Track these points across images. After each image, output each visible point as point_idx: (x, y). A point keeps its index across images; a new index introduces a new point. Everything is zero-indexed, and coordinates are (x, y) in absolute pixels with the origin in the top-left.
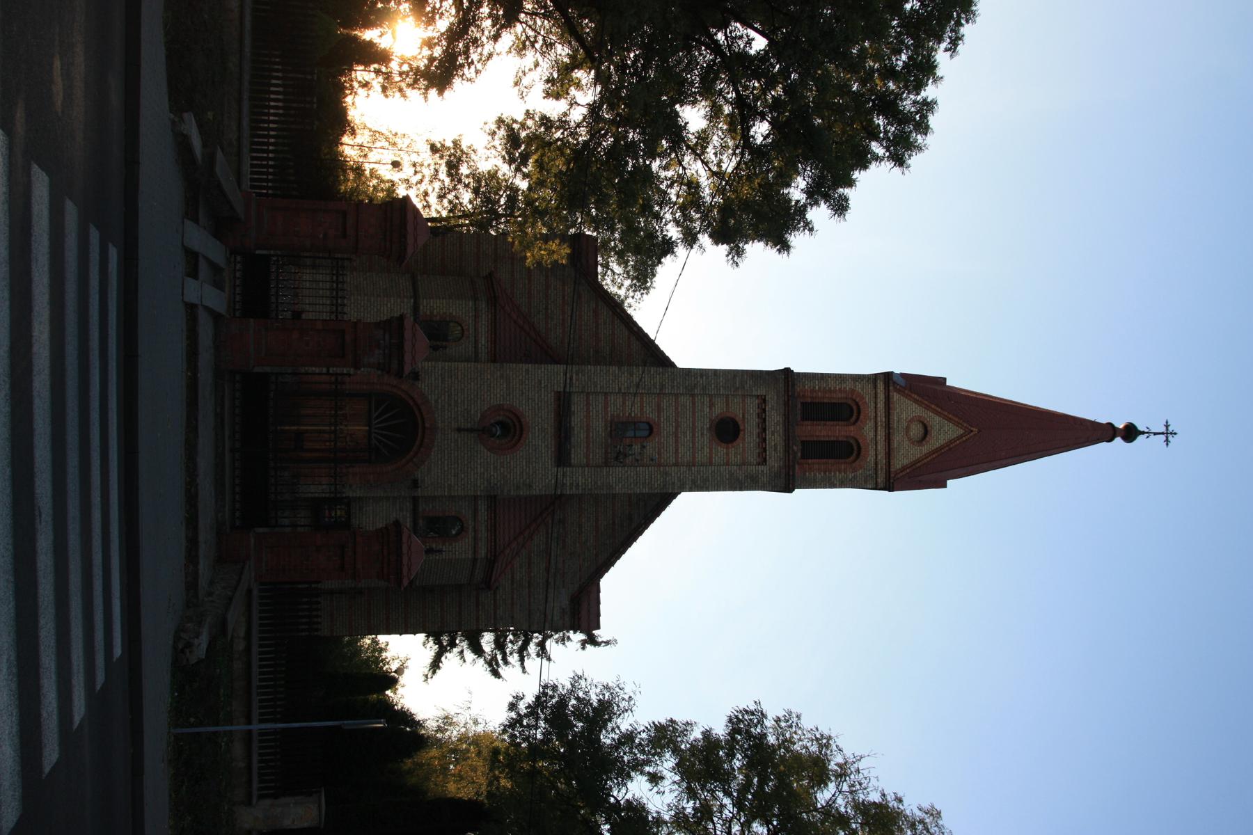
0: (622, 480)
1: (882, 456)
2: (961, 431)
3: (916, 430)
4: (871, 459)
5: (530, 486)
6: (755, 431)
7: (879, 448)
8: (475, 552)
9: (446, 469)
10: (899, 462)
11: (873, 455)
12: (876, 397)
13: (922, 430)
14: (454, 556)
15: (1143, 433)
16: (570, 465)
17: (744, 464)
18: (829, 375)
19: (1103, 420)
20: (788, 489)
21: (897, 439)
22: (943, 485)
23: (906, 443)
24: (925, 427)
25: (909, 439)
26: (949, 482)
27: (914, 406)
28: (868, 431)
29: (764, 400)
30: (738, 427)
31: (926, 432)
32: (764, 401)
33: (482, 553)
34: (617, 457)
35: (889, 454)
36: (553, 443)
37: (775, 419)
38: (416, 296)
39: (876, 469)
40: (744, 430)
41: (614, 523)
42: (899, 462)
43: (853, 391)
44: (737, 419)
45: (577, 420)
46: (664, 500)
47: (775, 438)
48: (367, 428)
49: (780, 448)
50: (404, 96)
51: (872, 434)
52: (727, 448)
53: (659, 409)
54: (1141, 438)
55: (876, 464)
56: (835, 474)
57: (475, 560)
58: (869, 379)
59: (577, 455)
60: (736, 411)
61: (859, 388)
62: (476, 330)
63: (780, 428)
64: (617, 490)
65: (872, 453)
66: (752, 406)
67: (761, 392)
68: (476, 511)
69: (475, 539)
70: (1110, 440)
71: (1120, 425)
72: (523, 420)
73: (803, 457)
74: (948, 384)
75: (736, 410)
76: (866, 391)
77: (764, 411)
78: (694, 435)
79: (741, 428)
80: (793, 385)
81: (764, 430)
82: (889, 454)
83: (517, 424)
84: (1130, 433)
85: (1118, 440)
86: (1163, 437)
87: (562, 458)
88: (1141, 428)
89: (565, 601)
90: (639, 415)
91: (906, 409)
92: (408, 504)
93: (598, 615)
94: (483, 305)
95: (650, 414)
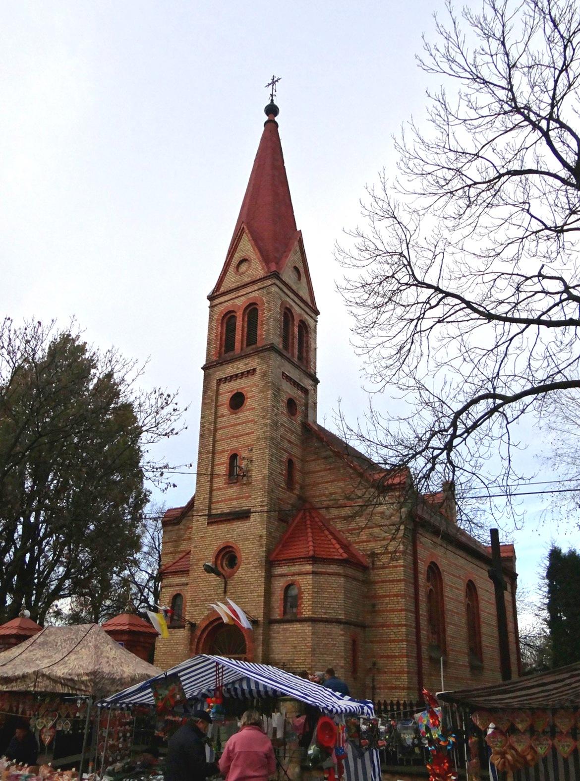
4: (256, 294)
5: (261, 536)
6: (239, 381)
7: (250, 290)
8: (307, 573)
9: (247, 600)
12: (221, 303)
14: (310, 590)
15: (272, 100)
18: (209, 339)
32: (220, 380)
33: (309, 568)
36: (235, 523)
39: (263, 288)
40: (238, 389)
41: (329, 469)
43: (217, 320)
44: (231, 396)
49: (246, 361)
51: (242, 298)
52: (247, 398)
53: (223, 451)
54: (275, 102)
56: (264, 317)
57: (314, 573)
58: (212, 311)
61: (216, 317)
63: (236, 364)
64: (266, 472)
68: (282, 575)
69: (299, 574)
70: (276, 125)
72: (222, 547)
75: (225, 398)
77: (226, 378)
78: (239, 424)
79: (236, 391)
80: (213, 362)
81: (237, 375)
83: (223, 553)
84: (272, 110)
87: (243, 515)
88: (269, 102)
90: (225, 465)
92: (275, 627)
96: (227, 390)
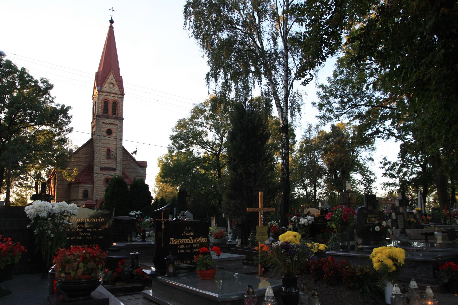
0: (120, 157)
1: (117, 96)
2: (112, 74)
3: (111, 86)
4: (117, 98)
6: (110, 125)
10: (119, 92)
11: (115, 98)
13: (111, 84)
16: (116, 168)
17: (117, 129)
20: (123, 119)
21: (113, 91)
22: (122, 77)
23: (114, 89)
24: (111, 83)
25: (113, 88)
26: (121, 75)
27: (105, 85)
28: (111, 98)
29: (103, 123)
34: (115, 159)
35: (116, 94)
37: (107, 121)
38: (78, 200)
42: (119, 92)
45: (106, 166)
46: (124, 149)
47: (112, 121)
49: (114, 120)
53: (104, 147)
54: (113, 19)
55: (118, 97)
59: (114, 166)
60: (105, 130)
61: (101, 99)
62: (86, 187)
63: (110, 120)
65: (116, 98)
66: (104, 126)
67: (101, 123)
73: (116, 115)
76: (102, 97)
80: (100, 115)
82: (116, 94)
84: (112, 22)
88: (110, 19)
89: (141, 169)
91: (106, 87)
93: (144, 162)
94: (80, 185)
95: (105, 150)
96: (105, 127)
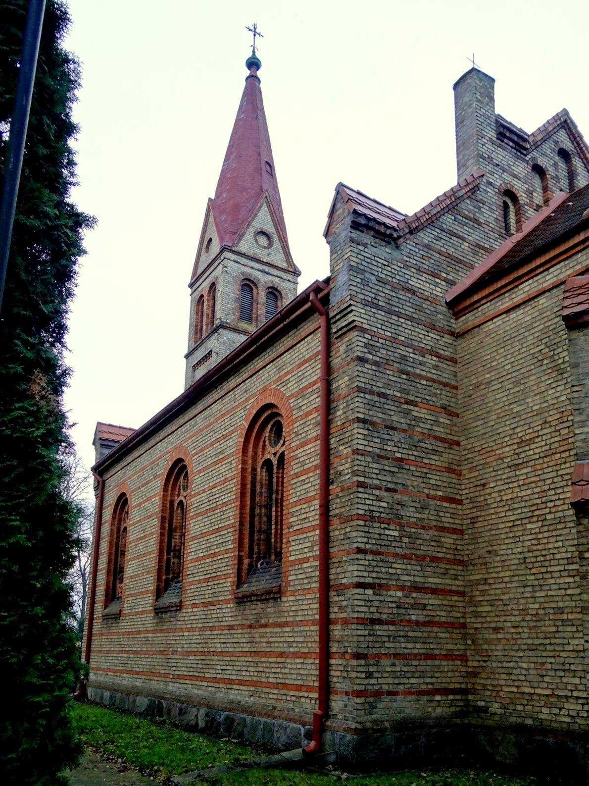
3: (263, 241)
15: (254, 52)
19: (243, 84)
30: (282, 428)
31: (263, 233)
48: (201, 724)
50: (80, 459)
54: (258, 55)
71: (247, 73)
74: (213, 197)
84: (253, 64)
85: (259, 73)
86: (257, 36)
88: (250, 54)
